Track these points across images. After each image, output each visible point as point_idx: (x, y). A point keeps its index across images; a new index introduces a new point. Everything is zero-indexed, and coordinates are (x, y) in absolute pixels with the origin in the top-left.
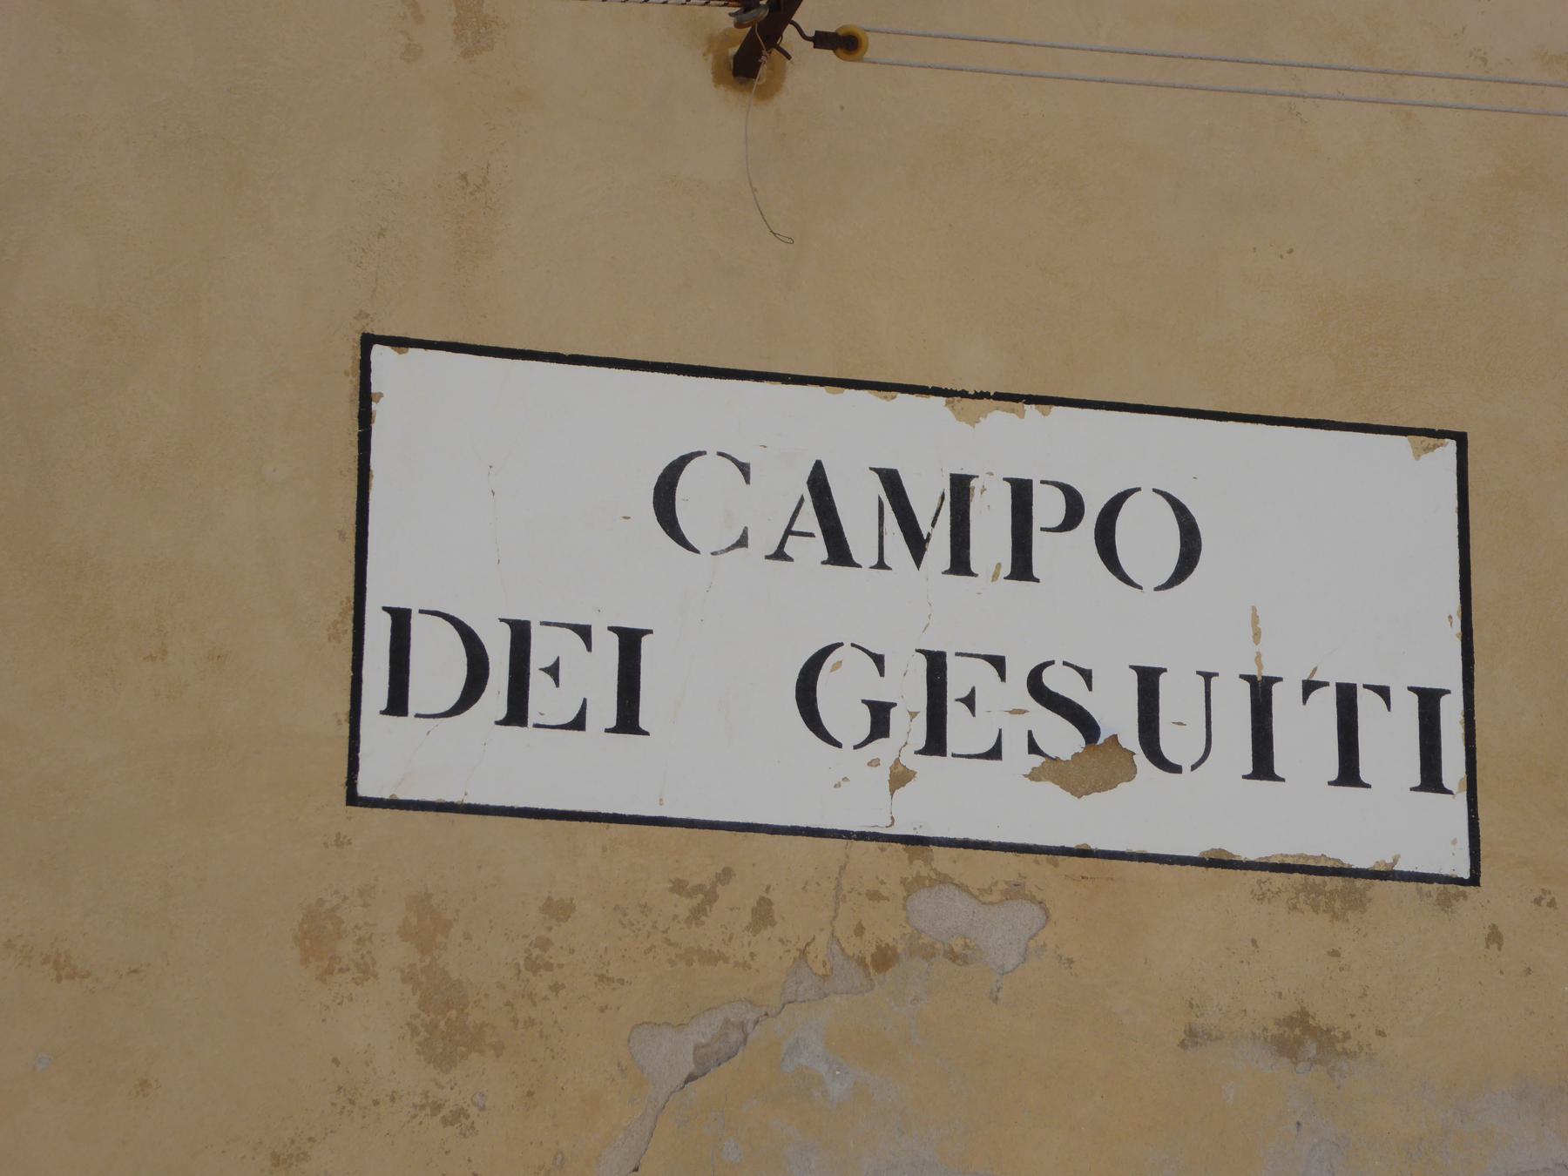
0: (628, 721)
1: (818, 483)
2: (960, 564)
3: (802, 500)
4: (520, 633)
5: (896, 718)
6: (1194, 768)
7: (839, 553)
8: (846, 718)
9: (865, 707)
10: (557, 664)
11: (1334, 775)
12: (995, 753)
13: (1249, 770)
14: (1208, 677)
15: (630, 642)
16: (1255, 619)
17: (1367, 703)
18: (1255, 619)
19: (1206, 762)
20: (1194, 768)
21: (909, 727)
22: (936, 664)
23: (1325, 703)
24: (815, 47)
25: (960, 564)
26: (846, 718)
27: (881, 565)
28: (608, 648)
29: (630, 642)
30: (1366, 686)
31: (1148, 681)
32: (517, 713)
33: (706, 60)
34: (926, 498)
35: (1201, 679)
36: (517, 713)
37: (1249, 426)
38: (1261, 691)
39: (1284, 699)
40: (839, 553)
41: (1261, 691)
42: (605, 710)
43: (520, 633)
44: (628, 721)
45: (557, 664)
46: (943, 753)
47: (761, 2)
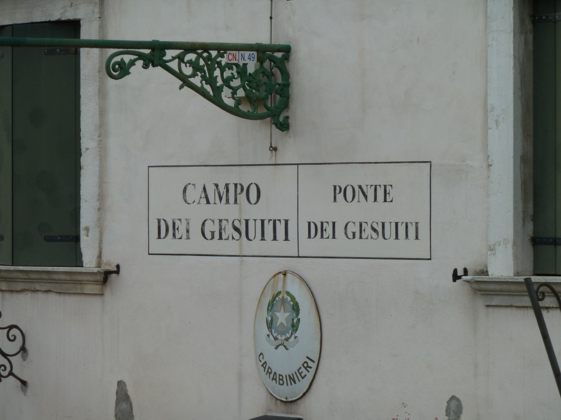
0: (334, 237)
1: (204, 189)
2: (227, 201)
5: (356, 234)
6: (254, 239)
7: (208, 202)
8: (350, 236)
9: (210, 232)
11: (284, 239)
13: (395, 238)
14: (391, 223)
17: (278, 222)
20: (254, 239)
24: (223, 91)
25: (227, 201)
26: (208, 235)
27: (215, 203)
31: (383, 224)
32: (322, 237)
33: (287, 118)
35: (254, 221)
36: (322, 237)
38: (397, 224)
40: (208, 202)
41: (397, 224)
42: (331, 236)
43: (322, 223)
44: (334, 237)
46: (222, 239)
47: (218, 85)
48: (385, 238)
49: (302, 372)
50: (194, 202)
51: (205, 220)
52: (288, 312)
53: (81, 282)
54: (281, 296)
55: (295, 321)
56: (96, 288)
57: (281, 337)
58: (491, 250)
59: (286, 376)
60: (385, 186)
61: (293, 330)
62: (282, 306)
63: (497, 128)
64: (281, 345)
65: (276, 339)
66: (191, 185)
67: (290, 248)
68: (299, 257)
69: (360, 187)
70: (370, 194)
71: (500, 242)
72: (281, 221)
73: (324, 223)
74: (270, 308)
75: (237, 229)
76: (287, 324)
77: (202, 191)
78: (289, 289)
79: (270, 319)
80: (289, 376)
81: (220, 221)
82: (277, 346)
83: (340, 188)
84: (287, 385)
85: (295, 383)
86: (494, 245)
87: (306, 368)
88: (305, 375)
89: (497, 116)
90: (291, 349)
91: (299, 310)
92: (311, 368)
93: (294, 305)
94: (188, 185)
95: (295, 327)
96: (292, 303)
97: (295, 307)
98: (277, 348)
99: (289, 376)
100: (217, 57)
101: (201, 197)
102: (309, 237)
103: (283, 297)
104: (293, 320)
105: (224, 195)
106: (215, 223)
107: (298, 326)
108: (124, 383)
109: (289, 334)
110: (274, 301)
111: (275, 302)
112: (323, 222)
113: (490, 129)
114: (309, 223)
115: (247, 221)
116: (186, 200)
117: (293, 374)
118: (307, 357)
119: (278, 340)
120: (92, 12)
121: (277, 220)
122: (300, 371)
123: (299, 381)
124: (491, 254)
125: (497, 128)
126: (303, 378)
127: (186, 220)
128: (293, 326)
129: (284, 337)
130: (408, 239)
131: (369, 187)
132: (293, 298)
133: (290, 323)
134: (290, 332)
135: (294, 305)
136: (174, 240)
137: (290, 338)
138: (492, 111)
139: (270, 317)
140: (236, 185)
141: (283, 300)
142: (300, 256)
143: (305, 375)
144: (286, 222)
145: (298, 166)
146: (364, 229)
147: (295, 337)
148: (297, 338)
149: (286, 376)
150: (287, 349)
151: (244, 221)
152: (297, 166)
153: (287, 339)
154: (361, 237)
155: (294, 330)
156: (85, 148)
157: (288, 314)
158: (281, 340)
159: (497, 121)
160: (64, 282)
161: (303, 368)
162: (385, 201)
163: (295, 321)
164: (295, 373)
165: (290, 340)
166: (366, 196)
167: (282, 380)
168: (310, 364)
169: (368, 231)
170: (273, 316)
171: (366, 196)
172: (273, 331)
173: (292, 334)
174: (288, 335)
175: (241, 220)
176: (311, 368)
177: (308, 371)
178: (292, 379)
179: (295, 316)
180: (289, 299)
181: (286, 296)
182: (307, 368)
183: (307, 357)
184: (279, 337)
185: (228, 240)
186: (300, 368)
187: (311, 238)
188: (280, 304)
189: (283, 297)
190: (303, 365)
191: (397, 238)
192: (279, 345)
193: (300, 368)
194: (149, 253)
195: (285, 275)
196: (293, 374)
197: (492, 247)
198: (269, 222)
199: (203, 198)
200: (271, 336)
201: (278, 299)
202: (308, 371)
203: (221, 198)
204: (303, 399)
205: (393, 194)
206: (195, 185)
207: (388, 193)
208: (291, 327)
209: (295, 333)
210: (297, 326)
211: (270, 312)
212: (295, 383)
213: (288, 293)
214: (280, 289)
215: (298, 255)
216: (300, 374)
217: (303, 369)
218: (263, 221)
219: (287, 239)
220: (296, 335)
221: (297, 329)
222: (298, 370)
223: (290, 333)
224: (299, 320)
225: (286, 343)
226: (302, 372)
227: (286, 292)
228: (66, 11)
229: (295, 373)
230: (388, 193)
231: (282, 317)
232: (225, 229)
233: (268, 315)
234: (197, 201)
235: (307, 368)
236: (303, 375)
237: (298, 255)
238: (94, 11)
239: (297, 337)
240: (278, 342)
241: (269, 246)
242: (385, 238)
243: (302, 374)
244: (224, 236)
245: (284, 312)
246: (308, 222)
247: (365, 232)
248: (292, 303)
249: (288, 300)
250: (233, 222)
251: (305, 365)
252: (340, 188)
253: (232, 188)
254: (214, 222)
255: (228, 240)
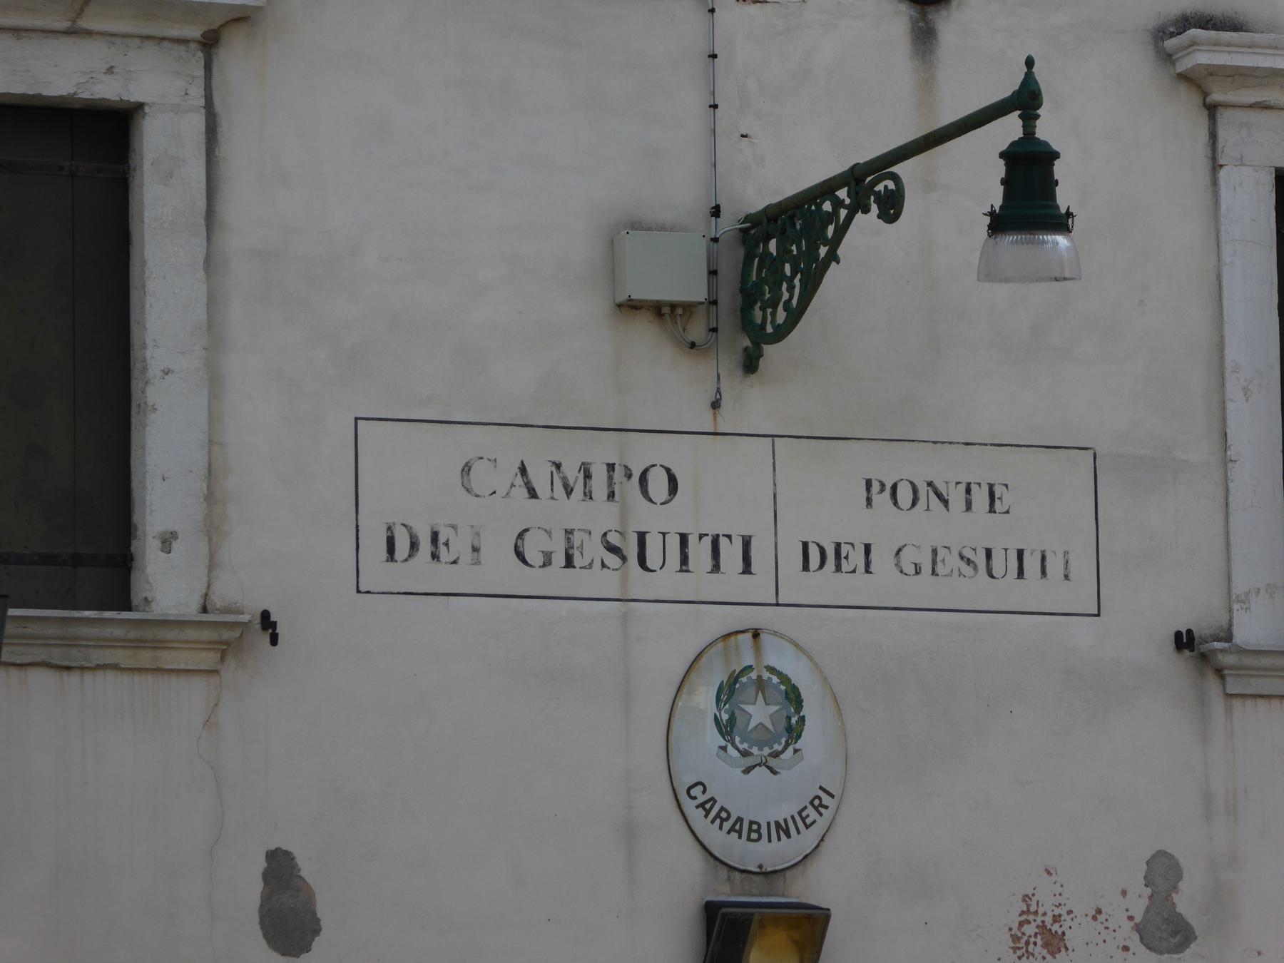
0: (867, 571)
2: (588, 495)
3: (552, 472)
4: (838, 547)
7: (533, 494)
8: (910, 569)
10: (448, 541)
12: (854, 571)
15: (868, 549)
16: (491, 494)
17: (723, 542)
18: (491, 494)
19: (665, 567)
21: (559, 559)
22: (935, 552)
23: (707, 541)
25: (588, 495)
26: (533, 555)
28: (861, 550)
29: (868, 549)
30: (723, 535)
32: (838, 568)
34: (572, 471)
35: (661, 535)
36: (838, 568)
37: (665, 429)
38: (1020, 554)
39: (692, 540)
40: (533, 494)
41: (684, 539)
42: (861, 567)
43: (838, 547)
44: (867, 571)
45: (448, 541)
48: (991, 576)
49: (808, 816)
50: (495, 492)
51: (527, 530)
52: (776, 704)
53: (158, 645)
54: (753, 675)
55: (794, 720)
56: (207, 659)
57: (760, 749)
58: (1240, 602)
59: (769, 824)
60: (991, 486)
61: (790, 737)
62: (760, 693)
63: (1247, 401)
64: (759, 765)
65: (745, 754)
66: (485, 461)
67: (758, 585)
68: (778, 605)
69: (930, 484)
70: (956, 497)
71: (1259, 589)
72: (733, 537)
73: (842, 545)
74: (726, 697)
75: (613, 549)
76: (773, 725)
77: (516, 474)
78: (772, 662)
79: (725, 717)
80: (777, 824)
81: (569, 532)
82: (749, 767)
83: (883, 485)
84: (770, 841)
85: (789, 836)
86: (1247, 594)
87: (816, 809)
88: (814, 822)
89: (1246, 380)
90: (784, 773)
91: (802, 701)
92: (826, 807)
93: (789, 691)
94: (476, 461)
95: (794, 732)
96: (783, 688)
97: (792, 696)
98: (747, 771)
99: (777, 824)
100: (845, 207)
101: (513, 485)
102: (806, 567)
103: (760, 677)
104: (789, 718)
105: (578, 482)
106: (552, 535)
107: (802, 731)
108: (287, 854)
109: (780, 744)
110: (735, 684)
111: (737, 686)
112: (840, 543)
113: (1232, 401)
114: (805, 546)
115: (642, 537)
116: (471, 488)
117: (785, 820)
118: (821, 788)
119: (750, 755)
120: (183, 94)
121: (721, 535)
122: (804, 814)
123: (799, 832)
124: (1240, 608)
125: (1247, 401)
126: (807, 827)
127: (472, 527)
128: (789, 729)
129: (767, 751)
130: (1047, 579)
131: (952, 485)
132: (784, 679)
133: (783, 723)
134: (783, 741)
135: (789, 691)
136: (435, 565)
137: (783, 751)
138: (1236, 372)
139: (725, 712)
140: (611, 467)
141: (760, 684)
142: (780, 602)
143: (814, 822)
144: (747, 543)
145: (773, 440)
146: (942, 559)
147: (796, 751)
148: (799, 753)
149: (769, 824)
150: (774, 772)
151: (635, 537)
152: (771, 439)
153: (776, 755)
154: (934, 572)
155: (793, 737)
156: (162, 368)
157: (774, 708)
158: (761, 756)
159: (1246, 390)
160: (126, 644)
161: (810, 807)
162: (992, 510)
163: (794, 720)
164: (793, 817)
165: (782, 756)
166: (945, 502)
167: (758, 831)
168: (826, 800)
169: (953, 562)
170: (737, 713)
171: (945, 502)
172: (737, 739)
173: (787, 745)
174: (778, 747)
175: (625, 532)
176: (826, 807)
177: (821, 814)
178: (782, 829)
179: (793, 710)
180: (775, 680)
181: (766, 675)
182: (820, 809)
183: (821, 788)
184: (755, 750)
185: (590, 568)
186: (805, 808)
187: (809, 571)
188: (752, 690)
189: (760, 677)
190: (812, 803)
191: (1021, 573)
192: (754, 766)
193: (805, 808)
194: (358, 587)
195: (756, 634)
196: (785, 820)
197: (1243, 597)
198: (700, 538)
199: (520, 486)
200: (730, 747)
201: (746, 680)
202: (821, 814)
203: (569, 491)
204: (800, 868)
205: (1006, 499)
206: (495, 460)
207: (998, 498)
208: (786, 733)
209: (795, 743)
210: (800, 729)
211: (725, 705)
212: (789, 836)
213: (772, 670)
214: (749, 659)
215: (777, 601)
216: (803, 820)
217: (811, 810)
218: (684, 539)
219: (747, 569)
220: (798, 746)
221: (799, 736)
222: (800, 813)
223: (784, 744)
224: (802, 719)
225: (772, 762)
226: (808, 816)
227: (765, 667)
228: (92, 80)
229: (793, 817)
230: (998, 498)
231: (759, 713)
232: (582, 549)
233: (720, 711)
234: (501, 492)
235: (820, 809)
236: (808, 821)
237: (777, 601)
238: (188, 92)
239: (800, 750)
240: (749, 761)
241: (700, 581)
242: (991, 576)
243: (806, 820)
244: (577, 561)
245: (766, 704)
246: (803, 542)
247: (944, 564)
248: (783, 688)
249: (773, 681)
250: (605, 534)
251: (816, 802)
252: (883, 485)
253: (599, 474)
254: (551, 533)
255: (590, 568)
